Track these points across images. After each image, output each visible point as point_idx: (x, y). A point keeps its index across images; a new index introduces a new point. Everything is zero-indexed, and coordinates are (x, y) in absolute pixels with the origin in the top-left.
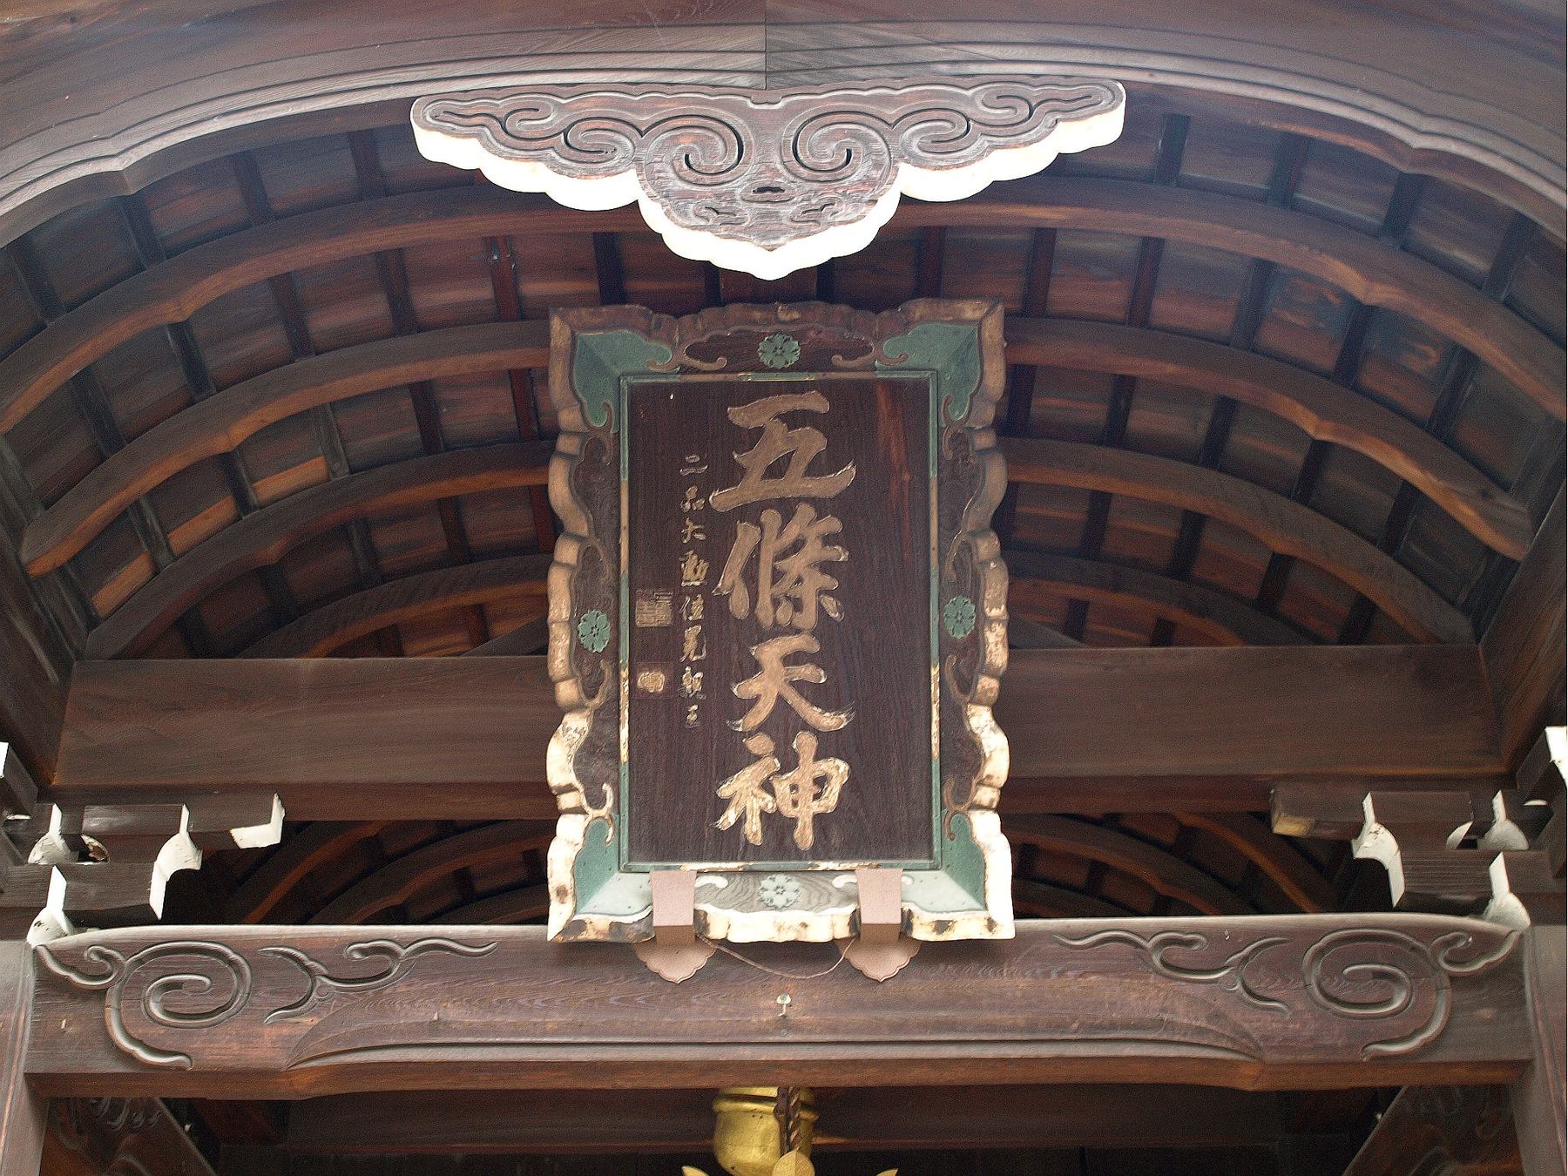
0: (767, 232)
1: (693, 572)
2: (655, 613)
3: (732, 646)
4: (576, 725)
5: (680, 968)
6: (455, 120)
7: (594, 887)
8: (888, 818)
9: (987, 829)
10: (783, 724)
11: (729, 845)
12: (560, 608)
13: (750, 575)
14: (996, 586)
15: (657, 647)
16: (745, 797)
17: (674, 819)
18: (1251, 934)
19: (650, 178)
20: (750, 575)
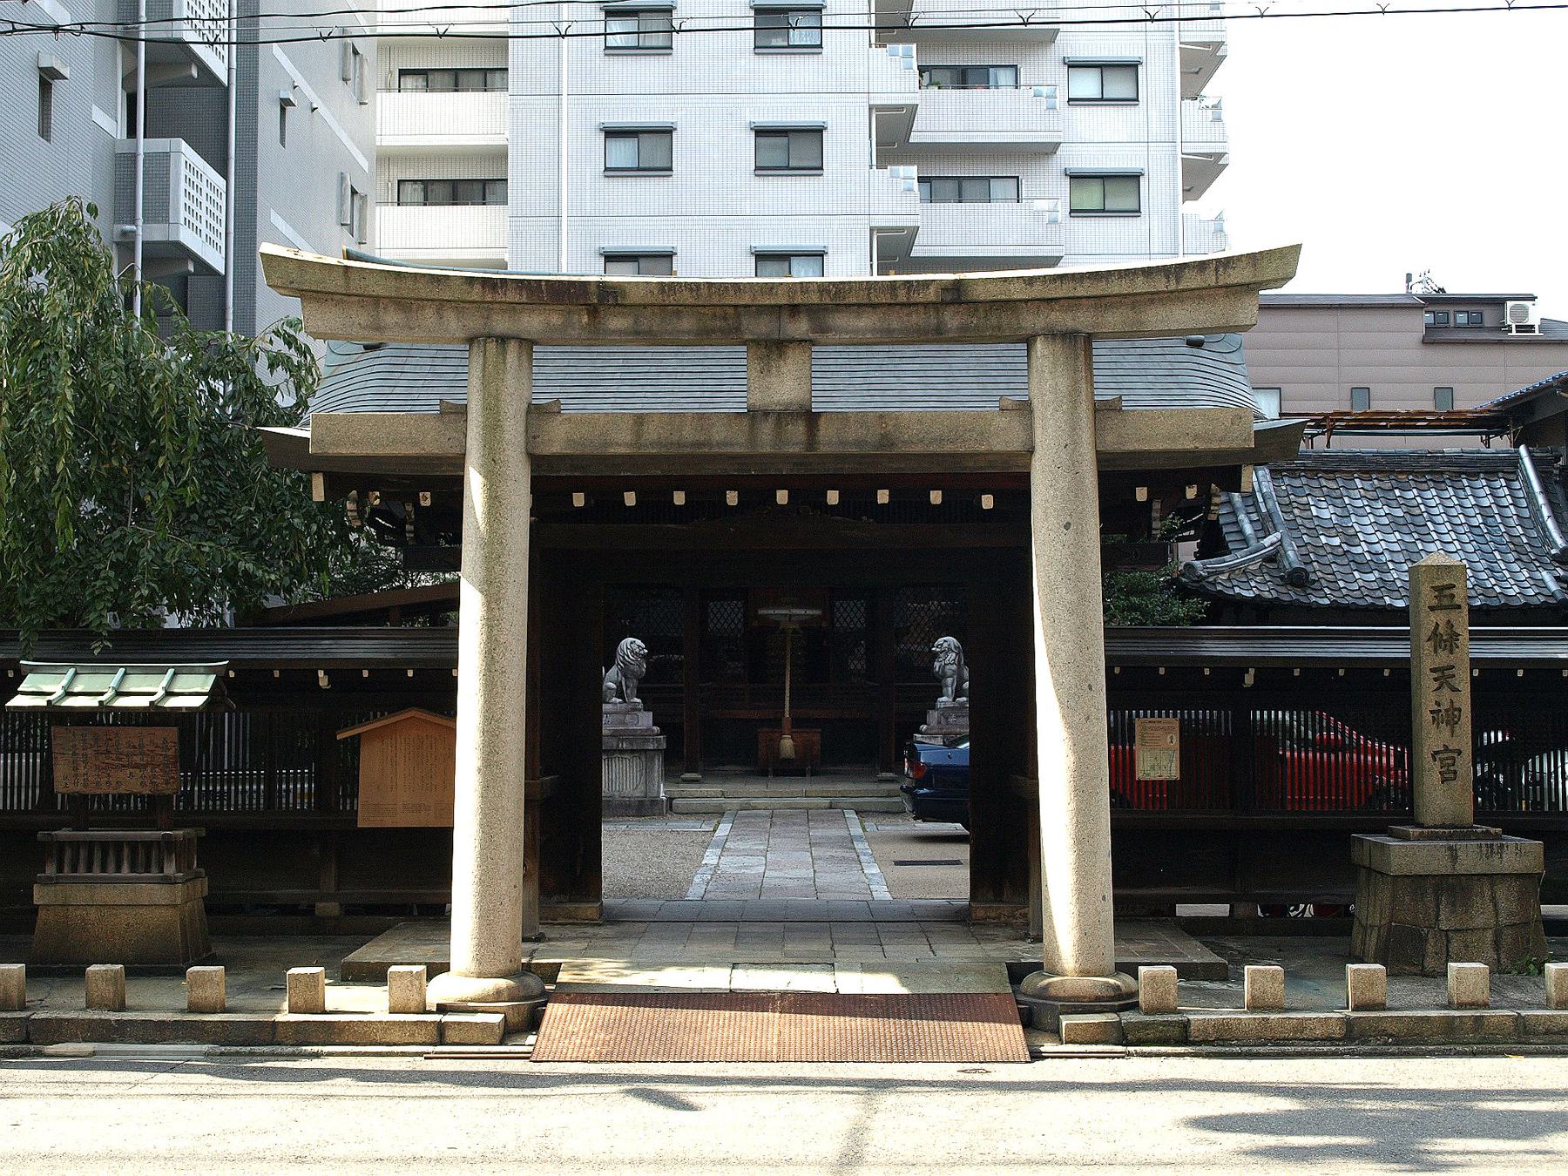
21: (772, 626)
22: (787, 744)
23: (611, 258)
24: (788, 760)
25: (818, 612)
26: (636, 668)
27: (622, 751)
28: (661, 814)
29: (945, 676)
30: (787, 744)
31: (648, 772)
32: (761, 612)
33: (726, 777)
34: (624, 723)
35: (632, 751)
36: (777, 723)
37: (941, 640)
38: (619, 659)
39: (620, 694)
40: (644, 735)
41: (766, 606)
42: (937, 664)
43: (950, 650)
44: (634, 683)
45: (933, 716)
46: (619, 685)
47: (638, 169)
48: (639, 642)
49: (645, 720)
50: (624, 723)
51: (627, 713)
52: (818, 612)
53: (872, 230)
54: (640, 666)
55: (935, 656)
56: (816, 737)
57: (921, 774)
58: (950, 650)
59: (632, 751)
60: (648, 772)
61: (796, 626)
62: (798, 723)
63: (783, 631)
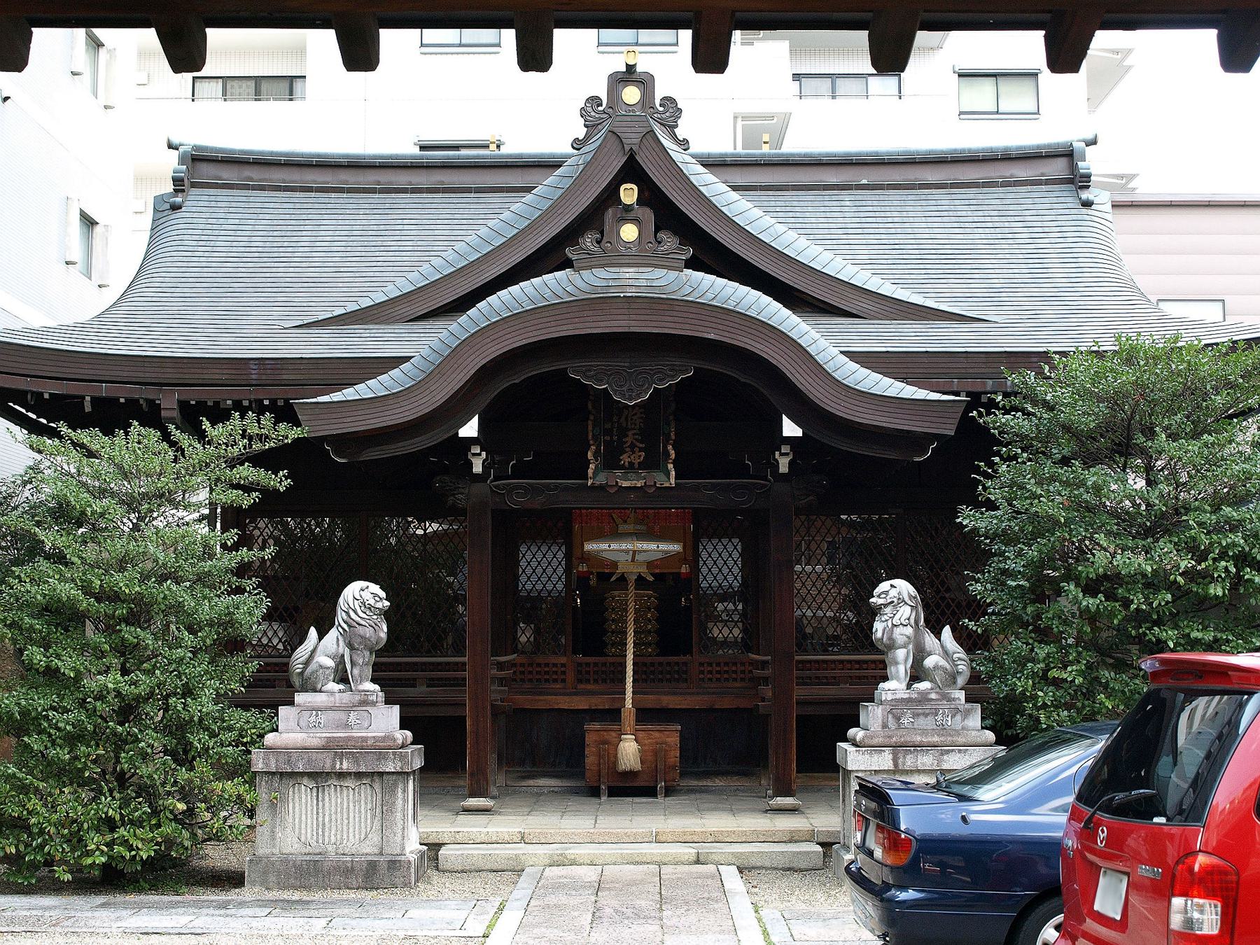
0: (630, 399)
1: (615, 419)
2: (608, 426)
3: (623, 432)
4: (593, 447)
5: (612, 491)
6: (577, 373)
7: (595, 475)
8: (653, 462)
9: (671, 466)
10: (632, 446)
11: (623, 467)
12: (590, 428)
13: (626, 419)
14: (673, 425)
15: (608, 432)
16: (625, 459)
17: (610, 462)
18: (719, 484)
19: (610, 385)
20: (626, 419)
21: (607, 578)
22: (629, 751)
23: (422, 148)
24: (631, 774)
25: (675, 547)
26: (368, 632)
27: (341, 775)
28: (406, 885)
29: (892, 646)
30: (629, 751)
31: (385, 812)
32: (590, 547)
33: (538, 800)
34: (347, 726)
35: (359, 775)
36: (613, 715)
37: (884, 586)
38: (340, 616)
39: (343, 679)
40: (382, 747)
41: (600, 536)
42: (878, 627)
43: (901, 601)
44: (365, 658)
45: (873, 716)
46: (340, 661)
47: (460, 45)
48: (375, 588)
49: (385, 721)
50: (347, 726)
51: (348, 709)
52: (675, 547)
53: (735, 118)
54: (375, 627)
55: (874, 612)
56: (671, 737)
57: (905, 859)
58: (901, 601)
59: (359, 775)
60: (385, 812)
61: (643, 570)
62: (645, 715)
63: (623, 579)
